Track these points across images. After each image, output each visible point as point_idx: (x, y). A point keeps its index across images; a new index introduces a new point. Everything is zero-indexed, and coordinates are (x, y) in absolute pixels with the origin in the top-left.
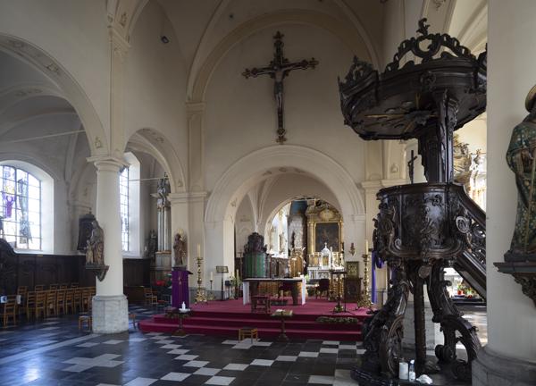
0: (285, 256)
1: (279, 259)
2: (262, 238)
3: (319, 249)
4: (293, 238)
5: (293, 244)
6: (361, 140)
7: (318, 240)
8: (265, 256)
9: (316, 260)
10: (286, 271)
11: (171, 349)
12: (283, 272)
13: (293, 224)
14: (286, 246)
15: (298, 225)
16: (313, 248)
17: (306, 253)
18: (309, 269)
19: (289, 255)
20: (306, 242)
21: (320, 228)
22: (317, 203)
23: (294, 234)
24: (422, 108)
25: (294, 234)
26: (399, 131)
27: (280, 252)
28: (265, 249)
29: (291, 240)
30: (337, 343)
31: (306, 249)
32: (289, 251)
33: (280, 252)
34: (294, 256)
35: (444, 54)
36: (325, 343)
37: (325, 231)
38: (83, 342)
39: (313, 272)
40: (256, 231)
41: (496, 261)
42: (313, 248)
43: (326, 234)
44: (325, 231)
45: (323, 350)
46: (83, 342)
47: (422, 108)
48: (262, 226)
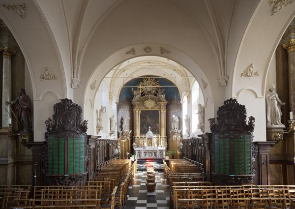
0: (114, 137)
1: (109, 140)
2: (79, 110)
3: (144, 131)
4: (122, 123)
5: (121, 127)
7: (142, 125)
8: (83, 138)
9: (141, 141)
10: (116, 151)
11: (189, 101)
12: (113, 152)
13: (121, 111)
14: (116, 129)
15: (126, 114)
16: (138, 131)
17: (133, 135)
18: (136, 149)
19: (118, 137)
20: (132, 126)
21: (144, 115)
22: (142, 93)
24: (96, 169)
25: (122, 119)
27: (111, 134)
28: (84, 128)
29: (120, 124)
30: (145, 202)
31: (133, 132)
32: (118, 133)
33: (111, 134)
34: (123, 138)
37: (148, 117)
39: (139, 152)
40: (69, 96)
41: (199, 134)
42: (138, 131)
43: (149, 120)
44: (148, 117)
47: (96, 169)
48: (80, 91)
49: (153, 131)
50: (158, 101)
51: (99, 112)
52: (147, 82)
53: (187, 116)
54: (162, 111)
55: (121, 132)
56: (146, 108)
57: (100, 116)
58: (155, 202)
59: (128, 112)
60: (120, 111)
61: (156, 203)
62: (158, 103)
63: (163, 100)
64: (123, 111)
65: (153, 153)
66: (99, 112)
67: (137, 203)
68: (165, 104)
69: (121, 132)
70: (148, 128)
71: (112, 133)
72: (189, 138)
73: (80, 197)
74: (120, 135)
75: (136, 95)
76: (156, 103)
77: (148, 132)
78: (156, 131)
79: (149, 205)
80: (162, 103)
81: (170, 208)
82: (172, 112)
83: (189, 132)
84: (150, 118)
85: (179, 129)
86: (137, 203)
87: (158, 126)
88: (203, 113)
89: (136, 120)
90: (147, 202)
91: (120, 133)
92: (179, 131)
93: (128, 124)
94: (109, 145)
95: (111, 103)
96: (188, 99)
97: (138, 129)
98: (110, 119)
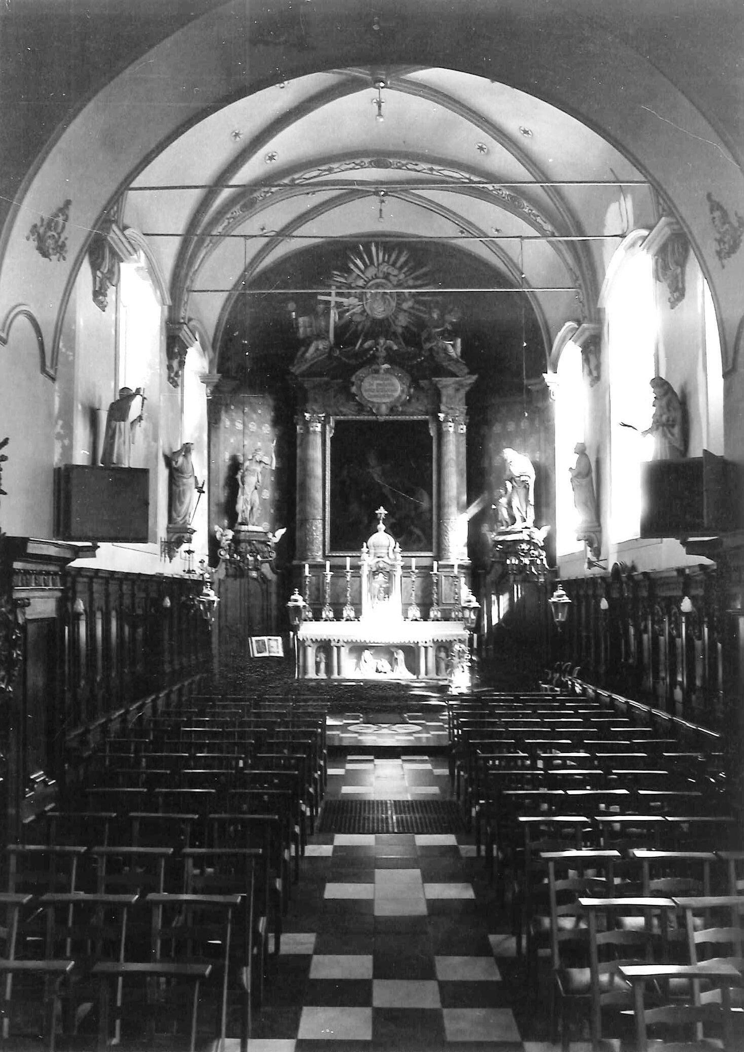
3: (349, 534)
4: (233, 485)
6: (684, 301)
15: (254, 437)
16: (319, 531)
17: (291, 550)
19: (214, 560)
21: (348, 446)
23: (235, 466)
25: (235, 466)
26: (113, 534)
27: (170, 548)
29: (222, 495)
30: (372, 757)
32: (214, 544)
35: (148, 737)
36: (349, 758)
37: (372, 461)
38: (479, 183)
42: (319, 531)
44: (372, 461)
45: (349, 766)
46: (479, 183)
49: (395, 530)
50: (422, 370)
51: (104, 416)
52: (371, 272)
53: (582, 451)
54: (450, 428)
55: (230, 534)
56: (361, 408)
57: (111, 436)
58: (427, 973)
59: (267, 429)
60: (226, 422)
61: (442, 985)
62: (423, 383)
63: (453, 368)
64: (239, 426)
65: (401, 656)
66: (104, 416)
67: (314, 974)
68: (460, 386)
69: (230, 534)
70: (375, 519)
71: (179, 542)
72: (596, 571)
73: (115, 944)
74: (224, 554)
75: (306, 342)
76: (415, 382)
77: (373, 539)
78: (418, 531)
79: (387, 994)
80: (447, 385)
81: (594, 1049)
82: (497, 428)
83: (593, 537)
84: (383, 457)
85: (537, 524)
86: (314, 974)
87: (425, 505)
88: (676, 430)
89: (306, 474)
90: (307, 958)
91: (225, 543)
92: (539, 536)
93: (267, 494)
94: (295, 629)
95: (174, 378)
96: (586, 360)
97: (319, 524)
98: (169, 461)
